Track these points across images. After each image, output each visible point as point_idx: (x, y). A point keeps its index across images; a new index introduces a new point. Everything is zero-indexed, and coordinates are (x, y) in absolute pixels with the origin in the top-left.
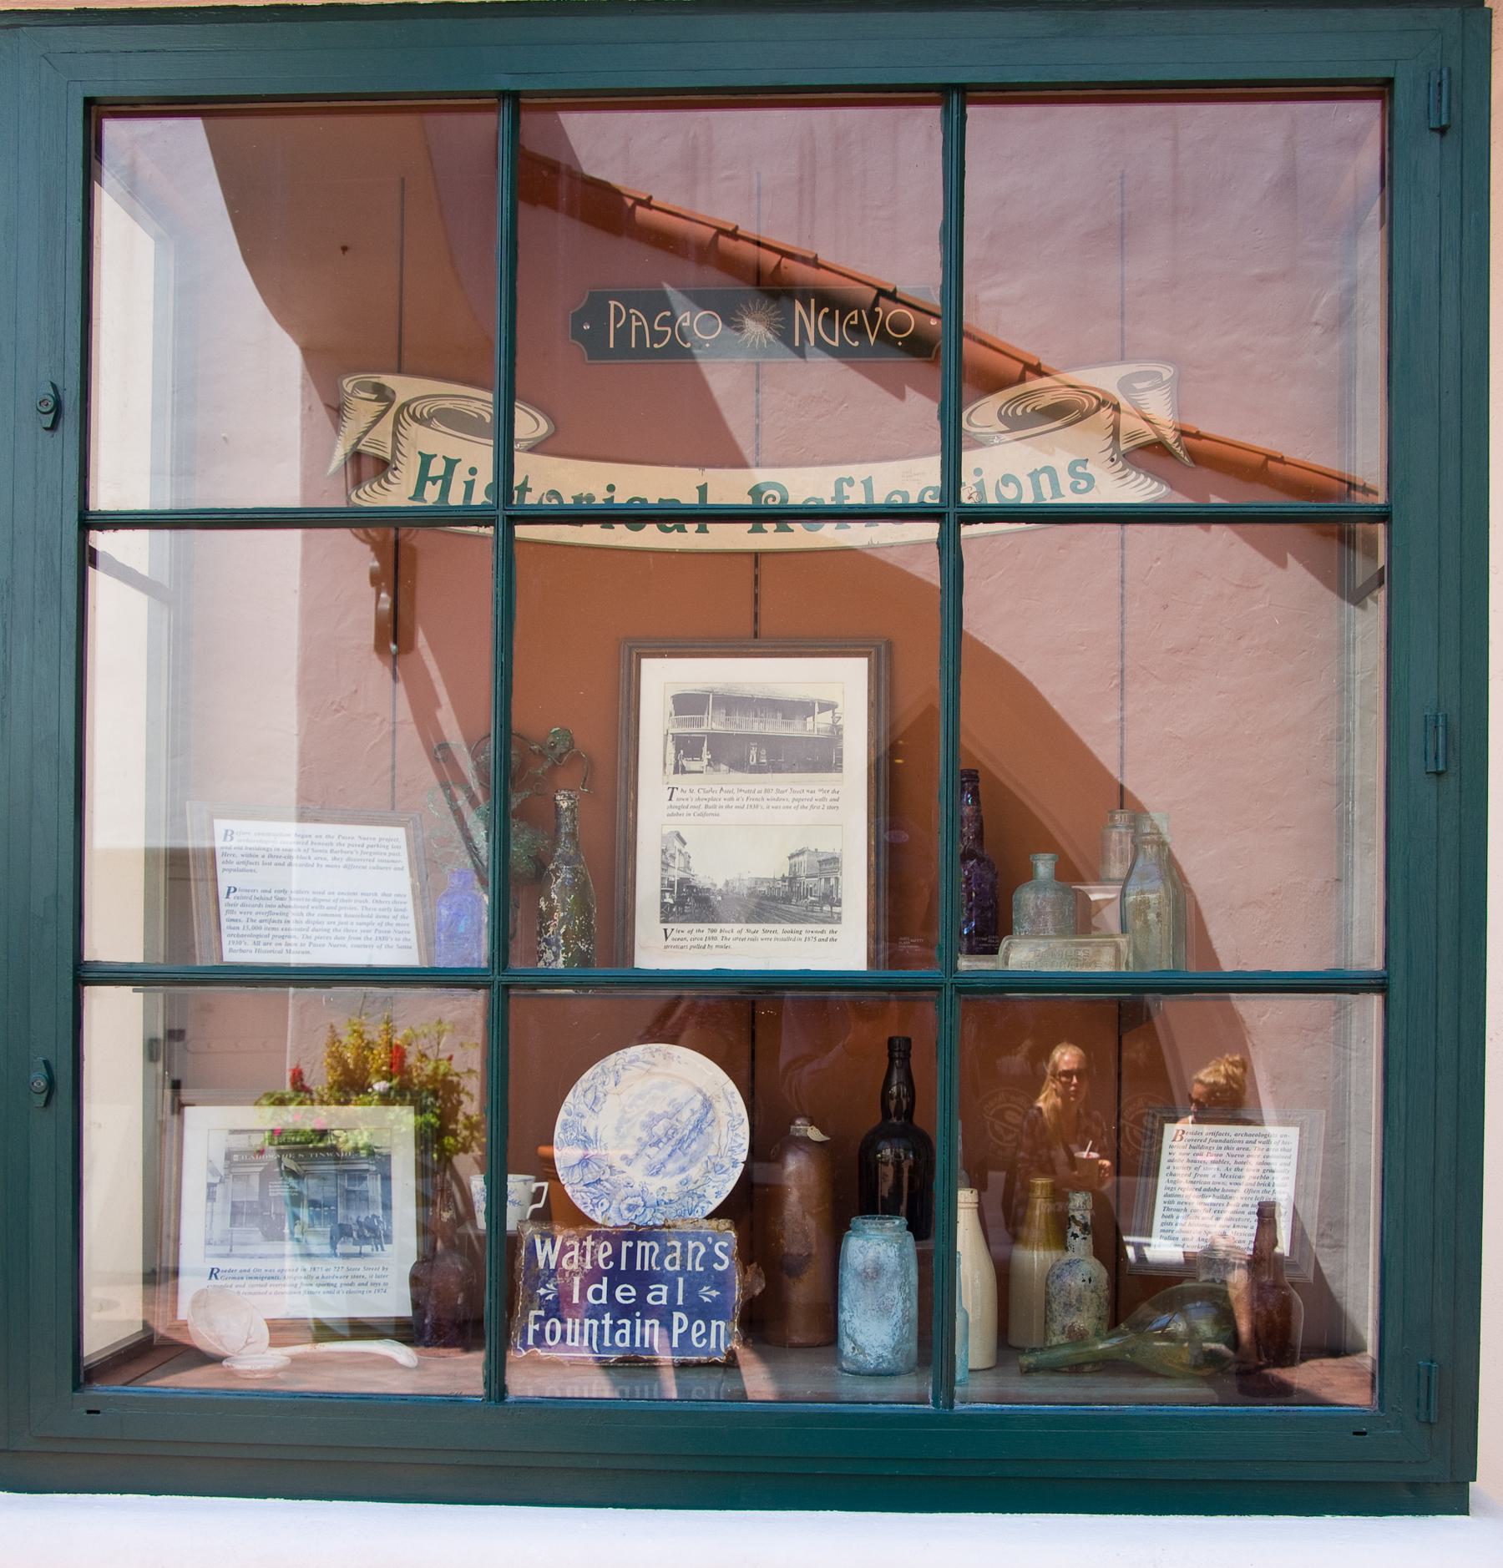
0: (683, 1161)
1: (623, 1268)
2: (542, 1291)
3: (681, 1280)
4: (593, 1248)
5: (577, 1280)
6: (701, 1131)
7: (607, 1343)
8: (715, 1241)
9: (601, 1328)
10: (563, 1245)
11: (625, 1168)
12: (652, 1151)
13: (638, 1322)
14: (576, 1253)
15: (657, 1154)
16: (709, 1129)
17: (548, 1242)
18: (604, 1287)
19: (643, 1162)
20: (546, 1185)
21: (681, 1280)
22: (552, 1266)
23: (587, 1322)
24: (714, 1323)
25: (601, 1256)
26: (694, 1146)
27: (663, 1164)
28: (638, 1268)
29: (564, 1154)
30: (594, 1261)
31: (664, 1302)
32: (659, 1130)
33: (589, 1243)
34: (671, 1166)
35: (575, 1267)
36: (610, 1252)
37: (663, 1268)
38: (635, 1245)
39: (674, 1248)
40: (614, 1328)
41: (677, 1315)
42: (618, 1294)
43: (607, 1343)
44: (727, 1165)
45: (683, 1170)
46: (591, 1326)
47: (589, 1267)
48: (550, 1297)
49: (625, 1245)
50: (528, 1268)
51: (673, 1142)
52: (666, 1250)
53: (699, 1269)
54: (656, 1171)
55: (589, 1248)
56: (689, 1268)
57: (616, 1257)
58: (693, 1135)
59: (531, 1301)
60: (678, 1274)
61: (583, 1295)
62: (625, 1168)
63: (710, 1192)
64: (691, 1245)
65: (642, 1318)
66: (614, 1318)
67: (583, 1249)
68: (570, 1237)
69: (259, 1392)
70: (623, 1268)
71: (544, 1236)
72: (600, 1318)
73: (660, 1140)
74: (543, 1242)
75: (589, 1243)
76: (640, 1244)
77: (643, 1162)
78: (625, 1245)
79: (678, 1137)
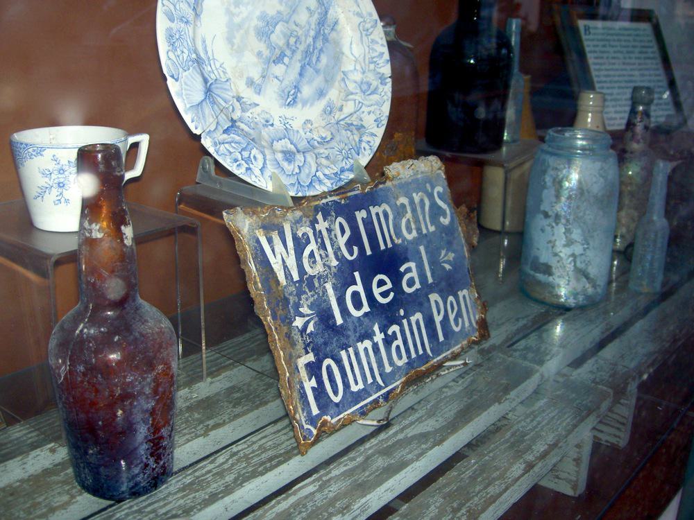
0: (319, 81)
1: (369, 252)
2: (299, 322)
3: (422, 248)
4: (329, 230)
5: (329, 286)
6: (326, 40)
7: (388, 369)
8: (433, 188)
9: (376, 347)
10: (295, 238)
11: (256, 99)
12: (278, 70)
13: (405, 321)
14: (312, 246)
15: (286, 72)
16: (334, 35)
17: (275, 237)
18: (359, 288)
19: (272, 89)
20: (144, 140)
21: (422, 248)
22: (296, 277)
23: (361, 346)
24: (461, 294)
25: (342, 241)
26: (324, 59)
27: (297, 88)
28: (383, 247)
29: (184, 93)
30: (337, 251)
31: (417, 286)
32: (277, 38)
33: (322, 225)
34: (307, 91)
35: (319, 268)
36: (348, 233)
37: (404, 239)
38: (369, 212)
39: (403, 206)
40: (388, 341)
41: (434, 297)
42: (376, 291)
43: (388, 369)
44: (375, 83)
45: (321, 94)
46: (366, 349)
47: (335, 263)
48: (311, 328)
49: (360, 215)
50: (268, 290)
51: (298, 56)
52: (399, 212)
53: (432, 229)
54: (291, 98)
55: (325, 233)
56: (424, 231)
57: (355, 240)
58: (319, 44)
59: (293, 344)
60: (417, 242)
61: (344, 312)
62: (256, 99)
63: (369, 121)
64: (417, 198)
65: (407, 316)
66: (384, 329)
67: (318, 235)
68: (298, 222)
69: (588, 476)
70: (369, 252)
71: (267, 228)
72: (369, 335)
73: (283, 55)
74: (270, 241)
75: (322, 225)
76: (374, 210)
77: (272, 89)
78: (360, 215)
79: (302, 47)
